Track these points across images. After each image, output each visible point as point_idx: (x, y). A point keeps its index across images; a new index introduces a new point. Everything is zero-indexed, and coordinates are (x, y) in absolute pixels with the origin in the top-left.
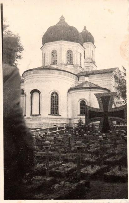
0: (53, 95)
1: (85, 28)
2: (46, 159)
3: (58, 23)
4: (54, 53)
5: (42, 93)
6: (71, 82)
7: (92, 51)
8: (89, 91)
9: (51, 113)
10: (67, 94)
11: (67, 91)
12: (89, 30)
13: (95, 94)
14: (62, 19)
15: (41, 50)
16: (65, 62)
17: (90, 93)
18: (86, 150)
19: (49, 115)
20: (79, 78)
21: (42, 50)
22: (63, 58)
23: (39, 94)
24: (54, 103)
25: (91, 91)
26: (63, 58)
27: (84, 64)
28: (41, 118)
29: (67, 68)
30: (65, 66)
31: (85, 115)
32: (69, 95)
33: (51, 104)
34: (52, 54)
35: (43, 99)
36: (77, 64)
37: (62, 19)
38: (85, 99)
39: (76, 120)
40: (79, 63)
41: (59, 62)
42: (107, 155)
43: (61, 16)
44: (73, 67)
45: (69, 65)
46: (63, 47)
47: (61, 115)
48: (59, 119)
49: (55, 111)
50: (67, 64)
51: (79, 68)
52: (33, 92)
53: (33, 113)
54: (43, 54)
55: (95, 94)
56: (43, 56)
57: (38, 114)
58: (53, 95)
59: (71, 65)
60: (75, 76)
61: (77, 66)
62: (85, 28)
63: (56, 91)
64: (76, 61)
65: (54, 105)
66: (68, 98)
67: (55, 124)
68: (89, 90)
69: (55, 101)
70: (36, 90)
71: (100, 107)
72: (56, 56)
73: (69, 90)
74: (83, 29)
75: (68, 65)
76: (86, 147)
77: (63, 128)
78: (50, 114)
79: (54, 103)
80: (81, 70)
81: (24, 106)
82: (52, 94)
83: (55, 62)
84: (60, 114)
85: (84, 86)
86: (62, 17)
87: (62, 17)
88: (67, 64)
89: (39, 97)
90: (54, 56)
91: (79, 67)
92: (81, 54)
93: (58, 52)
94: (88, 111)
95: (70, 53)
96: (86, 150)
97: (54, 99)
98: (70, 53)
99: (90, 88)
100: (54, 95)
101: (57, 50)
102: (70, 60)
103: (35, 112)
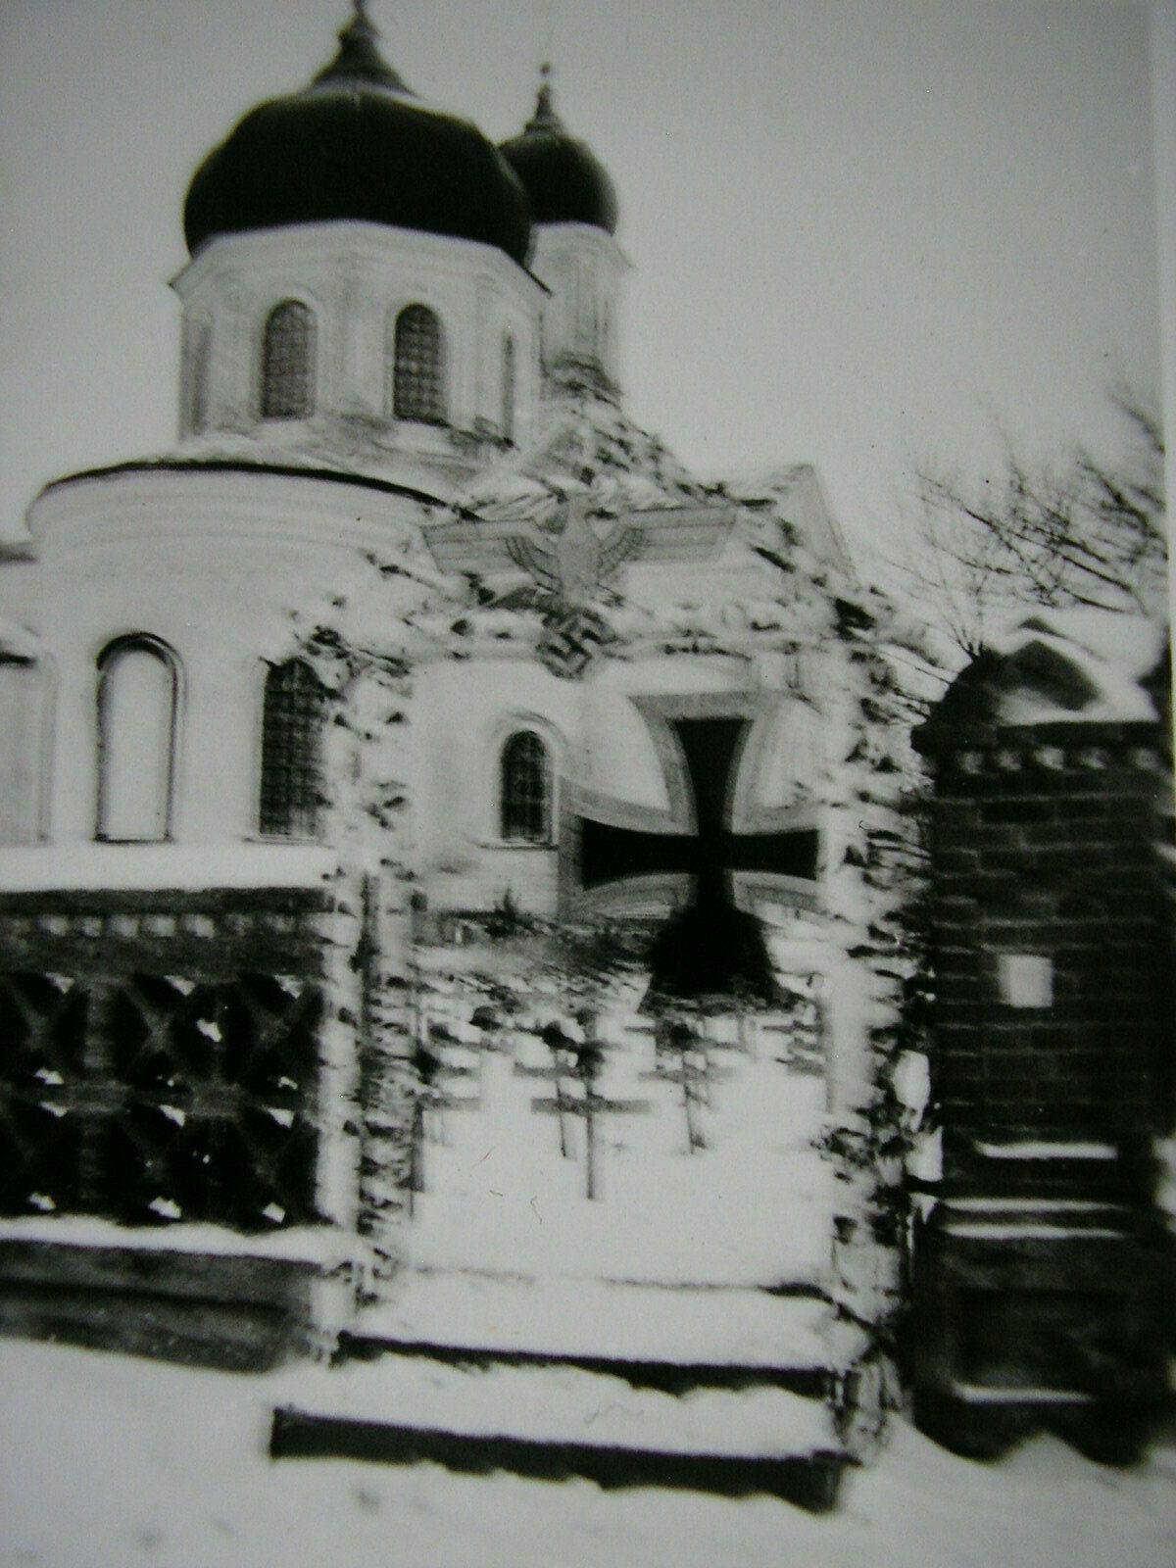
12: (577, 123)
13: (640, 703)
15: (170, 294)
18: (989, 765)
21: (182, 297)
22: (354, 365)
26: (354, 365)
31: (899, 1039)
38: (545, 722)
46: (355, 270)
52: (113, 650)
55: (640, 703)
58: (285, 686)
64: (466, 392)
71: (672, 799)
76: (972, 807)
81: (278, 840)
92: (509, 347)
93: (323, 319)
95: (415, 326)
96: (989, 765)
98: (415, 326)
102: (415, 395)
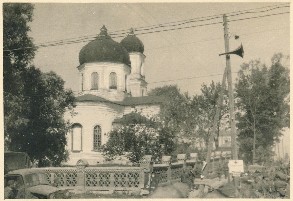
0: (96, 130)
2: (255, 167)
9: (94, 148)
19: (92, 151)
22: (105, 83)
28: (83, 154)
35: (85, 134)
37: (104, 30)
39: (85, 179)
41: (100, 86)
42: (203, 168)
43: (102, 26)
53: (75, 149)
60: (137, 80)
67: (98, 161)
73: (113, 122)
78: (93, 149)
82: (95, 128)
83: (95, 87)
86: (104, 27)
87: (104, 27)
93: (100, 75)
103: (77, 148)
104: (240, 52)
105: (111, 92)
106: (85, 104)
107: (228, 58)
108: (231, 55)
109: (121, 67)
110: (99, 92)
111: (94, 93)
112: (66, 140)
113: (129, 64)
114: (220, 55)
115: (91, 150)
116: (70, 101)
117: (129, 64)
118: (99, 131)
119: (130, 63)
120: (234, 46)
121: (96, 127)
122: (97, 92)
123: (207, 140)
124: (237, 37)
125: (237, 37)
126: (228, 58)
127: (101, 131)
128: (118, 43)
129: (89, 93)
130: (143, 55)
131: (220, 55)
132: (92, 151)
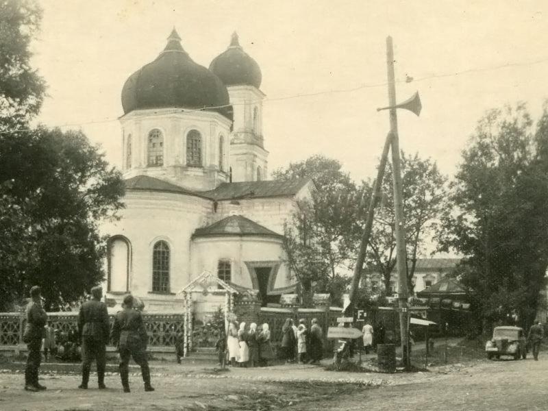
0: (158, 249)
1: (235, 41)
3: (162, 56)
4: (154, 135)
5: (134, 244)
6: (194, 214)
7: (255, 109)
8: (238, 241)
10: (188, 242)
11: (188, 236)
14: (174, 42)
16: (184, 162)
17: (241, 245)
19: (149, 293)
20: (215, 206)
22: (174, 150)
23: (127, 243)
24: (161, 266)
25: (242, 240)
27: (230, 146)
29: (188, 175)
30: (182, 173)
32: (194, 245)
33: (154, 268)
34: (150, 140)
36: (211, 166)
37: (174, 42)
40: (216, 163)
41: (168, 160)
44: (202, 174)
45: (193, 169)
47: (174, 294)
48: (171, 303)
49: (162, 283)
50: (189, 165)
51: (216, 174)
54: (126, 137)
56: (126, 141)
57: (126, 290)
59: (197, 169)
61: (211, 170)
62: (235, 41)
63: (164, 240)
64: (209, 156)
65: (161, 271)
66: (190, 254)
68: (238, 238)
69: (163, 262)
70: (122, 236)
72: (161, 144)
74: (229, 44)
75: (190, 169)
77: (216, 294)
78: (151, 291)
79: (161, 266)
80: (222, 178)
83: (157, 162)
84: (172, 291)
85: (229, 229)
88: (189, 165)
89: (126, 252)
90: (154, 144)
91: (218, 172)
94: (82, 359)
95: (194, 139)
97: (161, 258)
98: (194, 139)
99: (241, 235)
100: (161, 249)
101: (162, 130)
104: (414, 105)
105: (189, 173)
106: (147, 194)
107: (393, 115)
108: (399, 112)
109: (224, 126)
110: (164, 172)
111: (153, 173)
112: (269, 178)
113: (229, 112)
114: (379, 110)
115: (148, 291)
116: (113, 190)
117: (229, 112)
118: (163, 252)
119: (231, 108)
120: (402, 97)
121: (157, 245)
122: (161, 172)
123: (302, 177)
124: (409, 80)
125: (409, 80)
126: (393, 115)
127: (168, 253)
128: (205, 68)
129: (144, 174)
130: (260, 91)
131: (379, 110)
132: (149, 293)
